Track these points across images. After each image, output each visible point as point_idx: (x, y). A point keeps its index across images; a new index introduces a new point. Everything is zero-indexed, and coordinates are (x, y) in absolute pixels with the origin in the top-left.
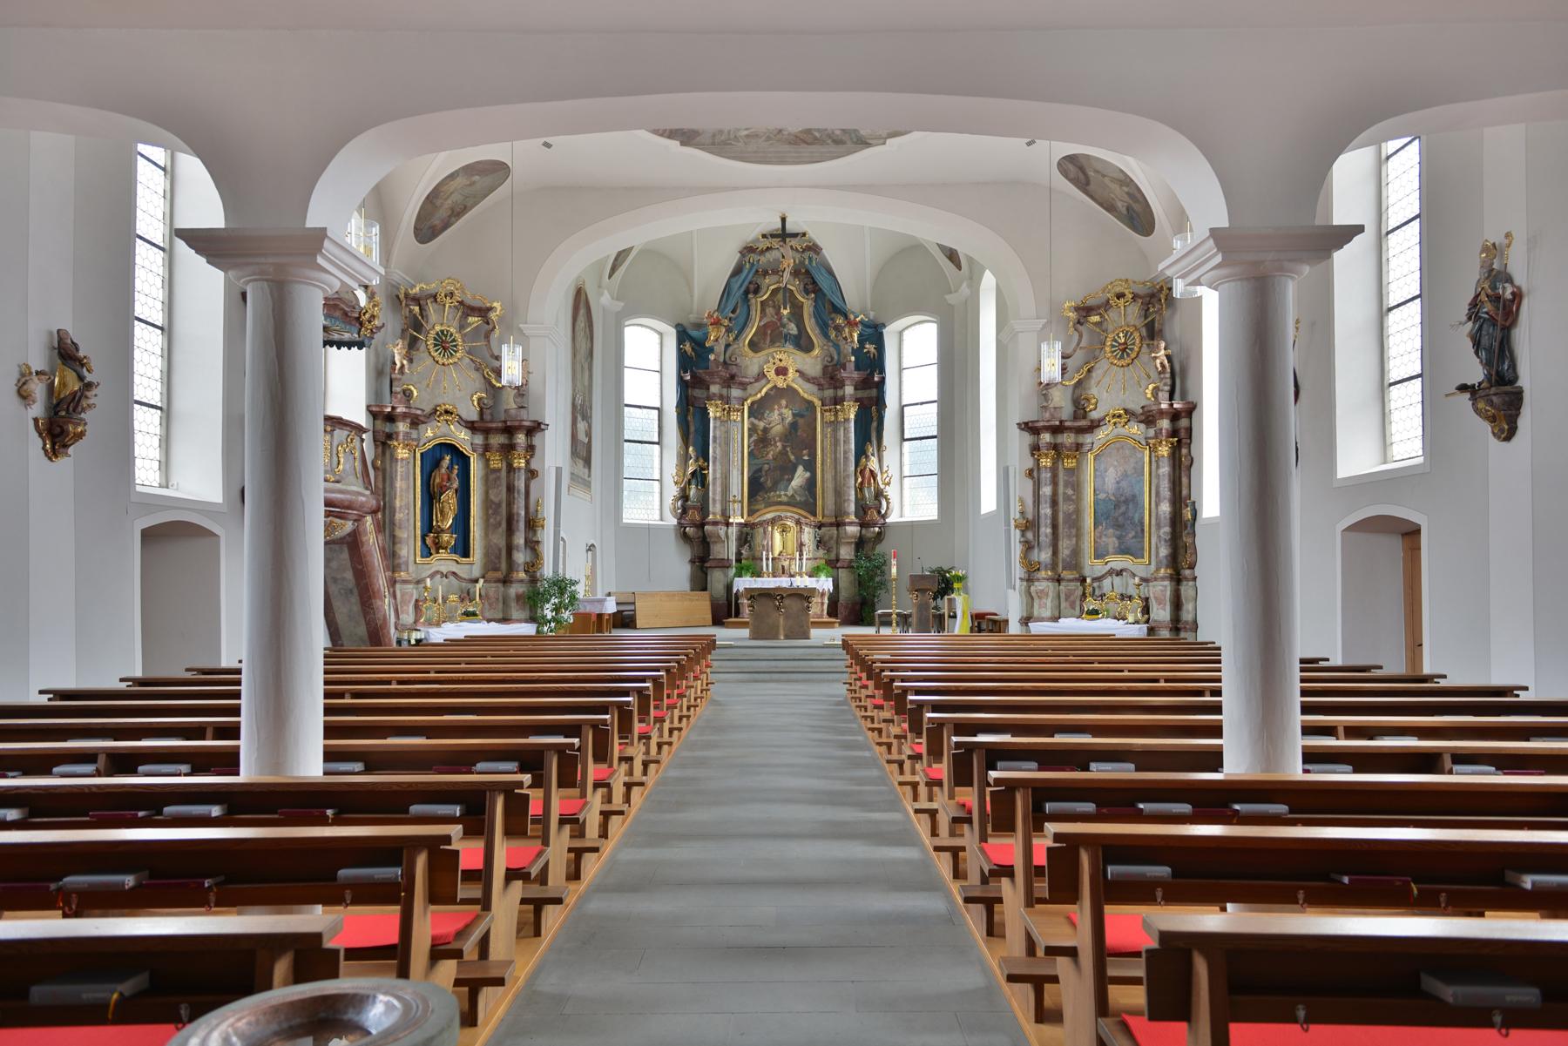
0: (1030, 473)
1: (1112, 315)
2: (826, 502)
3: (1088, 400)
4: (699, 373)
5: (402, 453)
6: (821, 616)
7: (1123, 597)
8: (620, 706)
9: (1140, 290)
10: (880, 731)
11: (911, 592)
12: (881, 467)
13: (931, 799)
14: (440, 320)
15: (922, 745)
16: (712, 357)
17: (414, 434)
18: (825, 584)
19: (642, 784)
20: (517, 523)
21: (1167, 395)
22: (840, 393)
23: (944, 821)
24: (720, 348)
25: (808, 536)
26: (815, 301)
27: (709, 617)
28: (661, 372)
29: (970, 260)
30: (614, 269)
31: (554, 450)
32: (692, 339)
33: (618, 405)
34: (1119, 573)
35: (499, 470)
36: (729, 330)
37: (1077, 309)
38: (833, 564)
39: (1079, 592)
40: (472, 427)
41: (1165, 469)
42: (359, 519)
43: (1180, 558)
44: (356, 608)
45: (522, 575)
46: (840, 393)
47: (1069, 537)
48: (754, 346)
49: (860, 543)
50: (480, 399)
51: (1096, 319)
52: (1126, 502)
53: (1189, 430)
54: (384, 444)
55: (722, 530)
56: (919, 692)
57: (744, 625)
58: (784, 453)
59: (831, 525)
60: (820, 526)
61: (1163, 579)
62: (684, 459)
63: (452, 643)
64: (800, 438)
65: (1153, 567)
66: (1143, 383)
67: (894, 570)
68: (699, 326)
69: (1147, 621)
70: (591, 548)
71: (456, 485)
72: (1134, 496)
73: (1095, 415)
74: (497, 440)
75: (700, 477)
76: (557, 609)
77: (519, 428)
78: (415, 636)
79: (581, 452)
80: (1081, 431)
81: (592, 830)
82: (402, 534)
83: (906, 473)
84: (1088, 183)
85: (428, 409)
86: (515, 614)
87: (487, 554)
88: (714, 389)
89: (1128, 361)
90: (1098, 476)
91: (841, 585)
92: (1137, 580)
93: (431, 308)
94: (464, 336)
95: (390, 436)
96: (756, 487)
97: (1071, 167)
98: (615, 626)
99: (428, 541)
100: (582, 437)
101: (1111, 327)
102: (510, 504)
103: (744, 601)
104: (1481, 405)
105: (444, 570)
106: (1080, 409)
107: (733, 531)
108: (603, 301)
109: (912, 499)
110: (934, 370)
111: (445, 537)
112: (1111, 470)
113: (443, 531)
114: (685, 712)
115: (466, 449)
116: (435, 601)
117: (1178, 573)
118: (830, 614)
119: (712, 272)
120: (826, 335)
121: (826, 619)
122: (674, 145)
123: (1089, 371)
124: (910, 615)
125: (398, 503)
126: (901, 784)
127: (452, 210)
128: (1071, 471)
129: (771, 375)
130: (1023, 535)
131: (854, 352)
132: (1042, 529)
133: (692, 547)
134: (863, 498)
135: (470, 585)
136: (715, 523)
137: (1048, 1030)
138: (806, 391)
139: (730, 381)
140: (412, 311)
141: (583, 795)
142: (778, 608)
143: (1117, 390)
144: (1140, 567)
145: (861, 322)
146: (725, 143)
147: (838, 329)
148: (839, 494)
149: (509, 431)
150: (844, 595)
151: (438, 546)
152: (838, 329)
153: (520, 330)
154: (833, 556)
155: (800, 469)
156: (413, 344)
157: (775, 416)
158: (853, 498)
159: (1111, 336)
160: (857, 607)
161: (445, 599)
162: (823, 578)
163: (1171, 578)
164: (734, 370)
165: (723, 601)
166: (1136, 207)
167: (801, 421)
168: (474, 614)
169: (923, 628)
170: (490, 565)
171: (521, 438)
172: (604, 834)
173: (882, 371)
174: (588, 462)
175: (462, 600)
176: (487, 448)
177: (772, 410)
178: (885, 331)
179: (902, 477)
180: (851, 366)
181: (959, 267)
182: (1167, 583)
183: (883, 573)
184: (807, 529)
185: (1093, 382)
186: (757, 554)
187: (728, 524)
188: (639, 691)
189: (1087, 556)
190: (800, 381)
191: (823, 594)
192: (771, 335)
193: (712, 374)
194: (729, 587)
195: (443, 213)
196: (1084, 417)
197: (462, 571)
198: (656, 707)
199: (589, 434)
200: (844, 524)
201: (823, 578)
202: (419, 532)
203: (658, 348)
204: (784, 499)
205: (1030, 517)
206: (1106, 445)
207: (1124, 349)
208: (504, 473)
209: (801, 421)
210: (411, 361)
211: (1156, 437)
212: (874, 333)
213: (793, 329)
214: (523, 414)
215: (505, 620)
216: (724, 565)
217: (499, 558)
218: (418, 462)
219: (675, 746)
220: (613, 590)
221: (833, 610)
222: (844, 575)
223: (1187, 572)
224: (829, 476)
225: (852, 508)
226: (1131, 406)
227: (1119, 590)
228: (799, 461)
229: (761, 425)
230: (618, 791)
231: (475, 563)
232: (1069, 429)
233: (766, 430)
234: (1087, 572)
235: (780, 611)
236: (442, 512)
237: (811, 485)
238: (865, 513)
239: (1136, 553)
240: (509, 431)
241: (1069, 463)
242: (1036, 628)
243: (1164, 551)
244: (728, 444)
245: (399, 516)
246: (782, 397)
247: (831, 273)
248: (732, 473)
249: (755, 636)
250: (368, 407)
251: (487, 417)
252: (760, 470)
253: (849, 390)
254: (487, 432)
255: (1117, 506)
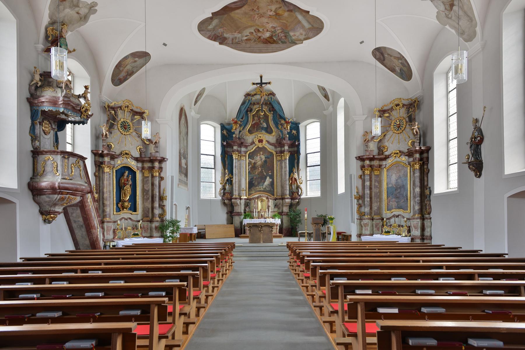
0: (361, 177)
1: (394, 113)
2: (278, 191)
3: (384, 147)
4: (229, 141)
5: (107, 170)
6: (276, 233)
7: (399, 226)
8: (203, 267)
9: (406, 102)
10: (293, 266)
11: (312, 224)
12: (299, 177)
13: (313, 291)
14: (123, 116)
15: (309, 273)
16: (234, 136)
17: (112, 162)
18: (278, 221)
19: (212, 296)
20: (155, 198)
21: (418, 144)
22: (283, 149)
23: (316, 298)
24: (237, 132)
25: (271, 203)
26: (273, 114)
27: (234, 234)
28: (215, 142)
29: (333, 93)
30: (196, 102)
31: (171, 169)
32: (226, 129)
33: (198, 154)
34: (398, 216)
35: (148, 177)
36: (240, 126)
37: (379, 111)
38: (281, 214)
39: (381, 224)
40: (137, 160)
41: (417, 174)
42: (82, 196)
43: (424, 210)
44: (85, 233)
45: (158, 219)
46: (283, 149)
47: (377, 202)
48: (250, 132)
49: (291, 206)
50: (140, 149)
51: (387, 115)
52: (400, 188)
53: (428, 158)
54: (99, 166)
55: (238, 201)
56: (314, 261)
57: (247, 237)
58: (262, 172)
59: (280, 199)
60: (276, 199)
61: (417, 219)
62: (224, 174)
63: (127, 247)
64: (268, 165)
65: (412, 214)
66: (407, 140)
67: (306, 216)
68: (229, 124)
69: (410, 236)
70: (188, 208)
71: (130, 183)
72: (403, 186)
73: (387, 153)
74: (147, 165)
75: (230, 181)
76: (173, 232)
77: (156, 160)
78: (112, 244)
79: (184, 171)
80: (381, 160)
81: (203, 301)
82: (107, 203)
83: (308, 179)
84: (384, 60)
85: (118, 153)
86: (155, 234)
87: (144, 211)
88: (235, 148)
89: (401, 131)
90: (388, 179)
91: (284, 221)
92: (405, 219)
93: (119, 112)
94: (133, 123)
95: (102, 163)
96: (251, 185)
97: (378, 53)
98: (197, 238)
99: (119, 205)
100: (183, 165)
101: (393, 118)
102: (153, 191)
103: (247, 228)
104: (471, 166)
105: (126, 217)
106: (381, 150)
107: (243, 202)
108: (191, 114)
109: (311, 189)
110: (319, 140)
111: (126, 204)
112: (394, 175)
113: (125, 201)
114: (230, 264)
115: (135, 169)
116: (122, 229)
117: (423, 216)
118: (280, 233)
119: (233, 103)
120: (277, 128)
121: (278, 234)
122: (216, 44)
123: (384, 136)
124: (312, 233)
125: (105, 190)
126: (302, 286)
127: (128, 72)
128: (377, 176)
129: (257, 142)
130: (358, 202)
131: (288, 133)
132: (366, 199)
133: (227, 208)
134: (292, 189)
135: (137, 223)
136: (236, 199)
137: (334, 334)
138: (270, 148)
139: (241, 145)
140: (111, 112)
141: (200, 290)
142: (260, 231)
143: (396, 144)
144: (407, 214)
145: (291, 122)
146: (237, 43)
147: (282, 125)
148: (283, 187)
149: (152, 161)
150: (285, 225)
151: (123, 208)
152: (282, 125)
153: (156, 121)
154: (281, 211)
155: (268, 178)
156: (111, 127)
157: (258, 158)
158: (288, 189)
159: (393, 122)
160: (290, 230)
161: (126, 229)
162: (277, 219)
163: (421, 218)
164: (243, 141)
165: (239, 228)
166: (405, 69)
167: (268, 160)
168: (137, 235)
169: (317, 239)
170: (145, 215)
171: (157, 164)
172: (206, 302)
173: (299, 140)
174: (186, 175)
175: (133, 229)
176: (143, 168)
177: (257, 156)
178: (300, 126)
179: (307, 181)
180: (287, 139)
181: (328, 100)
182: (419, 220)
183: (300, 217)
184: (270, 201)
185: (386, 140)
186: (252, 210)
187: (241, 199)
188: (211, 262)
189: (384, 210)
190: (268, 145)
191: (277, 225)
192: (256, 128)
193: (234, 142)
194: (241, 223)
195: (123, 74)
196: (383, 154)
197: (134, 217)
198: (217, 266)
199: (186, 164)
200: (285, 199)
201: (277, 219)
202: (115, 202)
203: (214, 133)
204: (262, 189)
205: (361, 194)
206: (392, 165)
207: (399, 127)
208: (150, 178)
209: (268, 160)
210: (111, 133)
211: (414, 161)
212: (296, 126)
213: (265, 125)
214: (157, 155)
215: (151, 237)
216: (239, 214)
217: (148, 212)
218: (115, 174)
219: (220, 288)
220: (197, 224)
221: (281, 231)
222: (285, 218)
223: (427, 216)
224: (279, 181)
225: (288, 192)
226: (402, 149)
227: (397, 223)
228: (268, 175)
229: (253, 161)
230: (210, 289)
231: (139, 215)
232: (377, 159)
233: (255, 163)
234: (384, 216)
235: (260, 232)
236: (125, 194)
237: (272, 184)
238: (293, 194)
239: (405, 208)
240: (152, 161)
241: (376, 173)
242: (364, 239)
243: (417, 207)
244: (240, 169)
245: (105, 195)
246: (261, 151)
247: (279, 104)
248: (241, 178)
249: (251, 241)
250: (92, 151)
251: (143, 156)
252: (253, 178)
253: (286, 148)
254: (143, 162)
255: (396, 190)
